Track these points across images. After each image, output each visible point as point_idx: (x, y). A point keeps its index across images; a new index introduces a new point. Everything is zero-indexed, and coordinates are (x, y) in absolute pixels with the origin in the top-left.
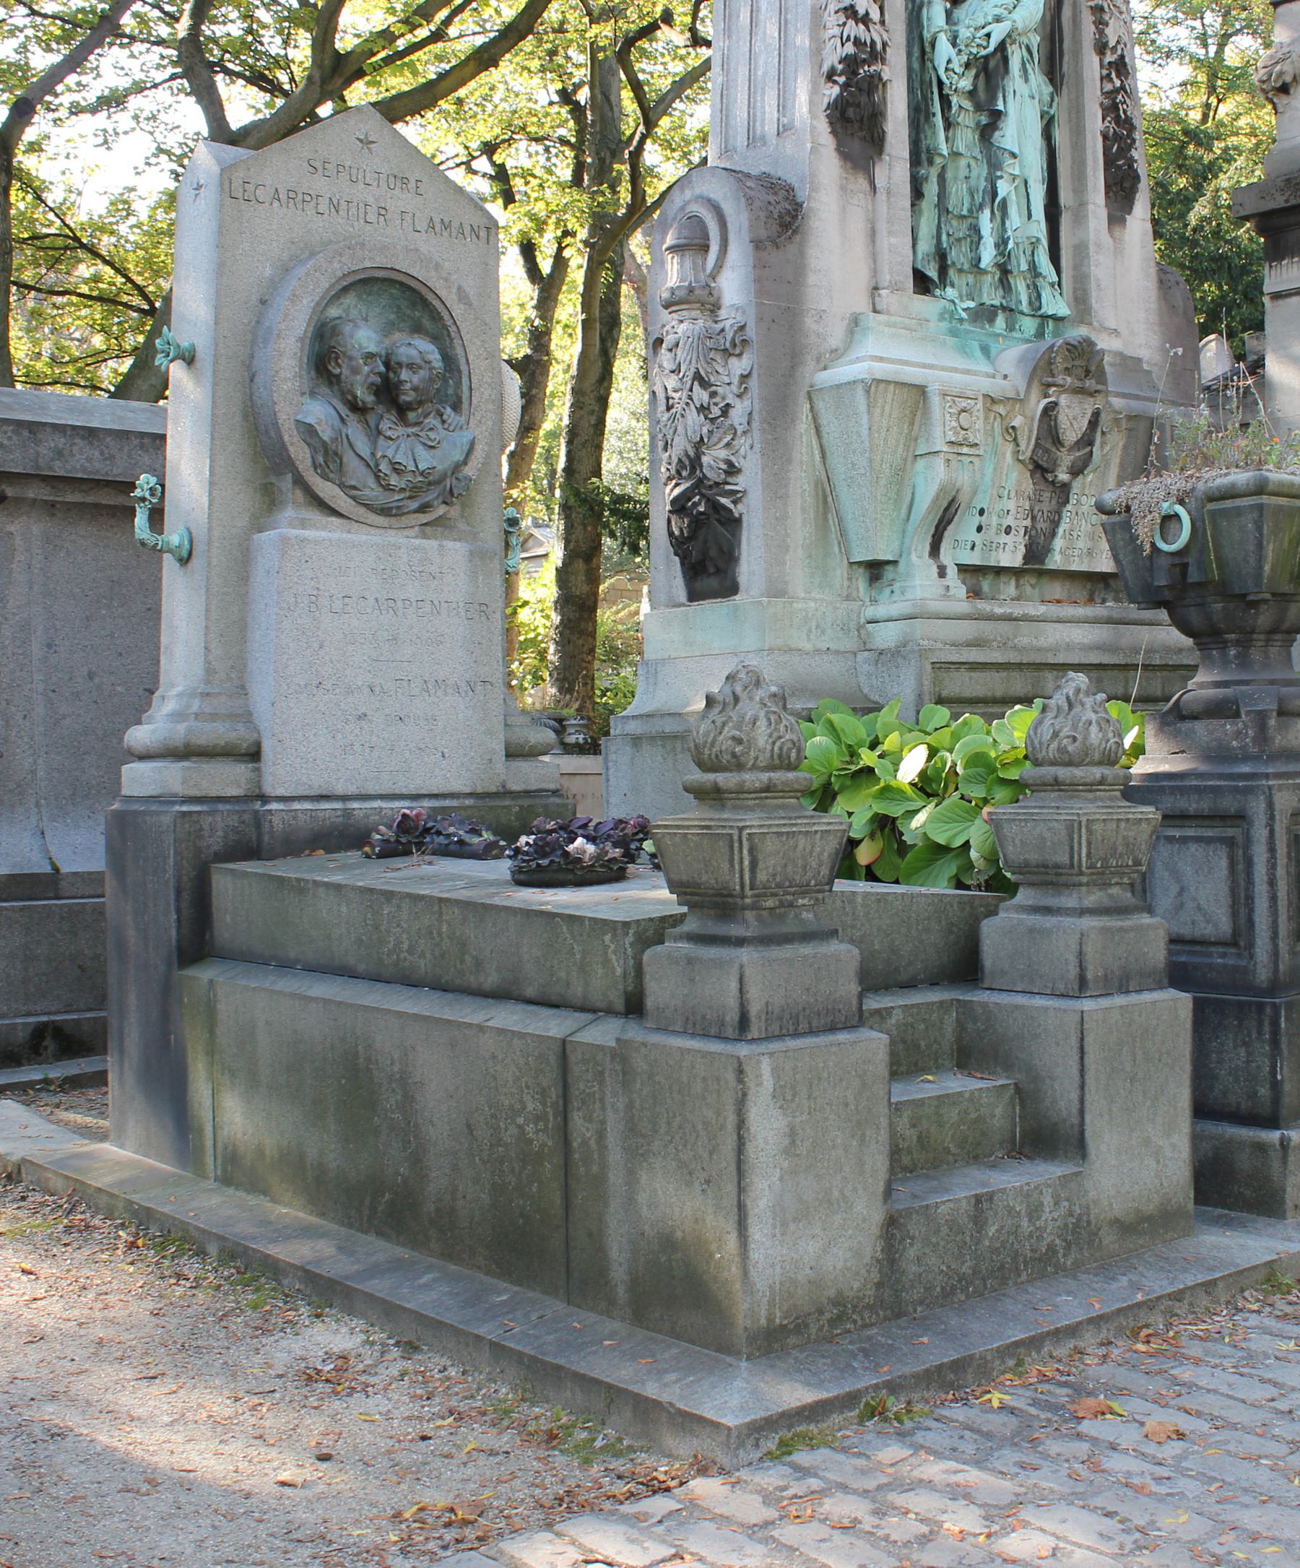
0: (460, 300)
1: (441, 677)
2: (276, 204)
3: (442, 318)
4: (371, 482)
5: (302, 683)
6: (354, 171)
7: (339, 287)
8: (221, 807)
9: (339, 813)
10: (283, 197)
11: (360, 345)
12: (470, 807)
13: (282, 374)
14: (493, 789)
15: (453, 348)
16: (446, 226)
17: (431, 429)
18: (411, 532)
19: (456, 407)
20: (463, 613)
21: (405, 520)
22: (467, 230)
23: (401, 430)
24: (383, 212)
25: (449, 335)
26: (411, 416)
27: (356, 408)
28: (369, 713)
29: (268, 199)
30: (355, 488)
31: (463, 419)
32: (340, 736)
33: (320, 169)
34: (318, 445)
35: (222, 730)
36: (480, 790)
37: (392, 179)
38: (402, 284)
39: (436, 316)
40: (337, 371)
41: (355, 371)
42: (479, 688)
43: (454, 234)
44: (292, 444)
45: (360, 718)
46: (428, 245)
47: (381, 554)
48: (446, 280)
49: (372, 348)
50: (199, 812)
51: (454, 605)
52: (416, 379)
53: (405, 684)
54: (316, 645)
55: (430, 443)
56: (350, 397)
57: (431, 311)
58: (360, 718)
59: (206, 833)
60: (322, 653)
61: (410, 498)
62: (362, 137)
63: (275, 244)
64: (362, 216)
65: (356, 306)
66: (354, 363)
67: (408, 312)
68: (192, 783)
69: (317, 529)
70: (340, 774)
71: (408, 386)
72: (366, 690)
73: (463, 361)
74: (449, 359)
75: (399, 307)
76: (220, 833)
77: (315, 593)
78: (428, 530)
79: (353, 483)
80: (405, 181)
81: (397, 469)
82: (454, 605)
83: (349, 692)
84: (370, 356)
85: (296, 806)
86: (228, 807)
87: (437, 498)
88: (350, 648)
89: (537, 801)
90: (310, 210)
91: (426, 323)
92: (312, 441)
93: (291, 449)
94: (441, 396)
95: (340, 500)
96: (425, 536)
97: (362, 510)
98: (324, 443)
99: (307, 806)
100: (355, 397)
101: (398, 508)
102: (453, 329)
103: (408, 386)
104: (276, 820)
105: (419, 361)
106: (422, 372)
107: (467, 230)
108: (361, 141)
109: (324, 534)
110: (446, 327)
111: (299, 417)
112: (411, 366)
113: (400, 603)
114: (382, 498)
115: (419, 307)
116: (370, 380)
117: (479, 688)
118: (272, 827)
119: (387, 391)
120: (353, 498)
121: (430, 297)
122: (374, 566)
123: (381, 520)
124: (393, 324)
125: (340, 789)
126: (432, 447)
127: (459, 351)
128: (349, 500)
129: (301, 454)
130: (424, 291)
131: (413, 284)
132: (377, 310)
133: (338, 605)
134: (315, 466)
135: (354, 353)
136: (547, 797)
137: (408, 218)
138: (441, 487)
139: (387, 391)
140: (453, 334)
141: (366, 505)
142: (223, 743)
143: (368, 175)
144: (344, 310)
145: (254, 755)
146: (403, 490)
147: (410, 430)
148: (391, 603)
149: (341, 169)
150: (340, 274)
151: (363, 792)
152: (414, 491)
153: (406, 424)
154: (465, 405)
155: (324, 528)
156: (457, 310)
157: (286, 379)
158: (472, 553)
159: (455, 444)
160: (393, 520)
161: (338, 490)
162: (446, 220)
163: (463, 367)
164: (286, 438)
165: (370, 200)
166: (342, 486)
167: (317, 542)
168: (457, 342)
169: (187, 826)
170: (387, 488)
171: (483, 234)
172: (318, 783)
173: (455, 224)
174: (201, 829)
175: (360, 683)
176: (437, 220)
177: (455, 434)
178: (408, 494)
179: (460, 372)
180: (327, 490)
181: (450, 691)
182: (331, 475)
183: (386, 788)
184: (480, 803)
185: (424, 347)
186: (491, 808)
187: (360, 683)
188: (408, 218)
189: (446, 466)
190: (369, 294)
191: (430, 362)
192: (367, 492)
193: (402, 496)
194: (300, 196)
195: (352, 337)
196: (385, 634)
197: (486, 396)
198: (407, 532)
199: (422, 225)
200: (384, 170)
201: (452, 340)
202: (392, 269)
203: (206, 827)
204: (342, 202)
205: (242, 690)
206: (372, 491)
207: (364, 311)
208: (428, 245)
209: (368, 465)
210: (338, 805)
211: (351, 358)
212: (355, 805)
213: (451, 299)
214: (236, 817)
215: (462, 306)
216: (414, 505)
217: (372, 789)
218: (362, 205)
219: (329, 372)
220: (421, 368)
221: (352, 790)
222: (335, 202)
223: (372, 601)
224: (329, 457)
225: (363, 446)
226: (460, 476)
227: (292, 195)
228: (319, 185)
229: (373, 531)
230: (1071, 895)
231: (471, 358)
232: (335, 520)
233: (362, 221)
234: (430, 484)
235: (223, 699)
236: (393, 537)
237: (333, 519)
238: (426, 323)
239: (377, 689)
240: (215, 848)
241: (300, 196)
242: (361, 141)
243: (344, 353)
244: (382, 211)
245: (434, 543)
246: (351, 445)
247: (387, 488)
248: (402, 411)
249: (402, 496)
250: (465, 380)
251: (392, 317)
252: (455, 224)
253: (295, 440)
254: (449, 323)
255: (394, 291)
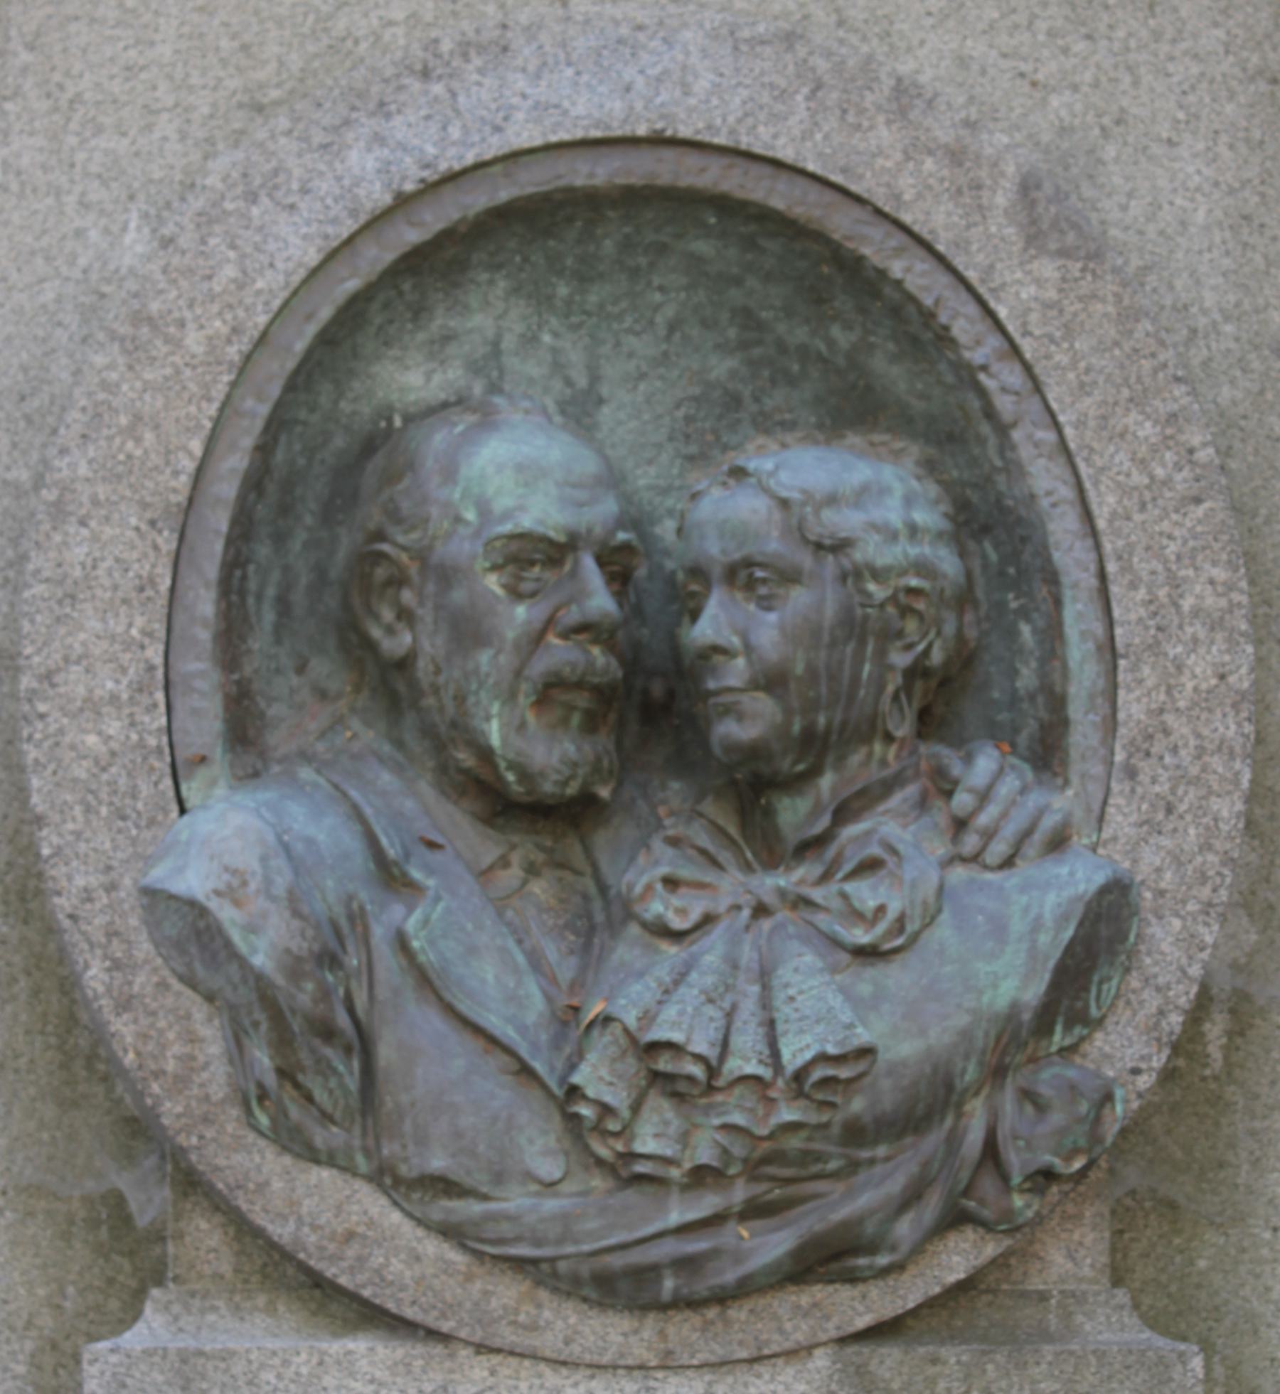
0: (1034, 238)
3: (944, 338)
4: (541, 1150)
7: (377, 256)
13: (75, 683)
15: (1014, 469)
17: (870, 866)
21: (746, 1324)
23: (733, 886)
25: (990, 413)
26: (793, 814)
30: (446, 1186)
31: (1061, 803)
34: (245, 995)
38: (725, 205)
39: (922, 335)
40: (397, 644)
41: (468, 631)
44: (125, 1004)
48: (956, 156)
49: (543, 513)
52: (769, 631)
55: (861, 936)
57: (895, 312)
61: (755, 1211)
63: (167, 126)
65: (530, 340)
66: (458, 596)
67: (800, 335)
73: (1062, 528)
74: (990, 521)
75: (746, 317)
79: (438, 1163)
81: (661, 1071)
84: (533, 556)
87: (911, 1198)
91: (893, 373)
92: (215, 982)
93: (123, 1028)
94: (943, 701)
95: (398, 1252)
97: (507, 1292)
98: (260, 983)
100: (486, 754)
101: (687, 1264)
102: (1002, 381)
103: (736, 672)
105: (774, 545)
110: (968, 376)
111: (158, 875)
112: (744, 575)
115: (843, 303)
116: (540, 666)
119: (647, 702)
120: (450, 1232)
121: (874, 246)
123: (609, 1331)
124: (734, 401)
127: (1044, 478)
128: (432, 1247)
130: (842, 223)
131: (779, 196)
132: (645, 346)
134: (252, 1097)
135: (461, 548)
138: (933, 1140)
139: (647, 702)
140: (1005, 405)
144: (474, 368)
146: (701, 1176)
147: (770, 883)
150: (377, 195)
152: (772, 1175)
153: (769, 849)
154: (1083, 732)
156: (1024, 288)
157: (92, 707)
159: (999, 929)
160: (683, 1327)
161: (371, 1204)
163: (1071, 557)
164: (95, 976)
166: (387, 1179)
168: (1029, 440)
170: (629, 1174)
177: (1010, 880)
178: (740, 1193)
179: (1052, 578)
180: (317, 1204)
182: (321, 1137)
185: (878, 499)
189: (940, 1035)
190: (583, 279)
191: (841, 546)
192: (515, 1200)
193: (707, 1203)
195: (450, 474)
197: (1201, 667)
201: (1003, 430)
202: (658, 141)
206: (541, 1186)
207: (575, 357)
209: (525, 1071)
215: (1048, 268)
216: (771, 1245)
219: (370, 645)
220: (790, 577)
225: (503, 984)
230: (741, 1307)
231: (1104, 505)
234: (855, 1133)
238: (893, 373)
243: (422, 556)
246: (426, 981)
247: (629, 1174)
249: (707, 1203)
250: (1078, 616)
251: (721, 367)
255: (703, 247)
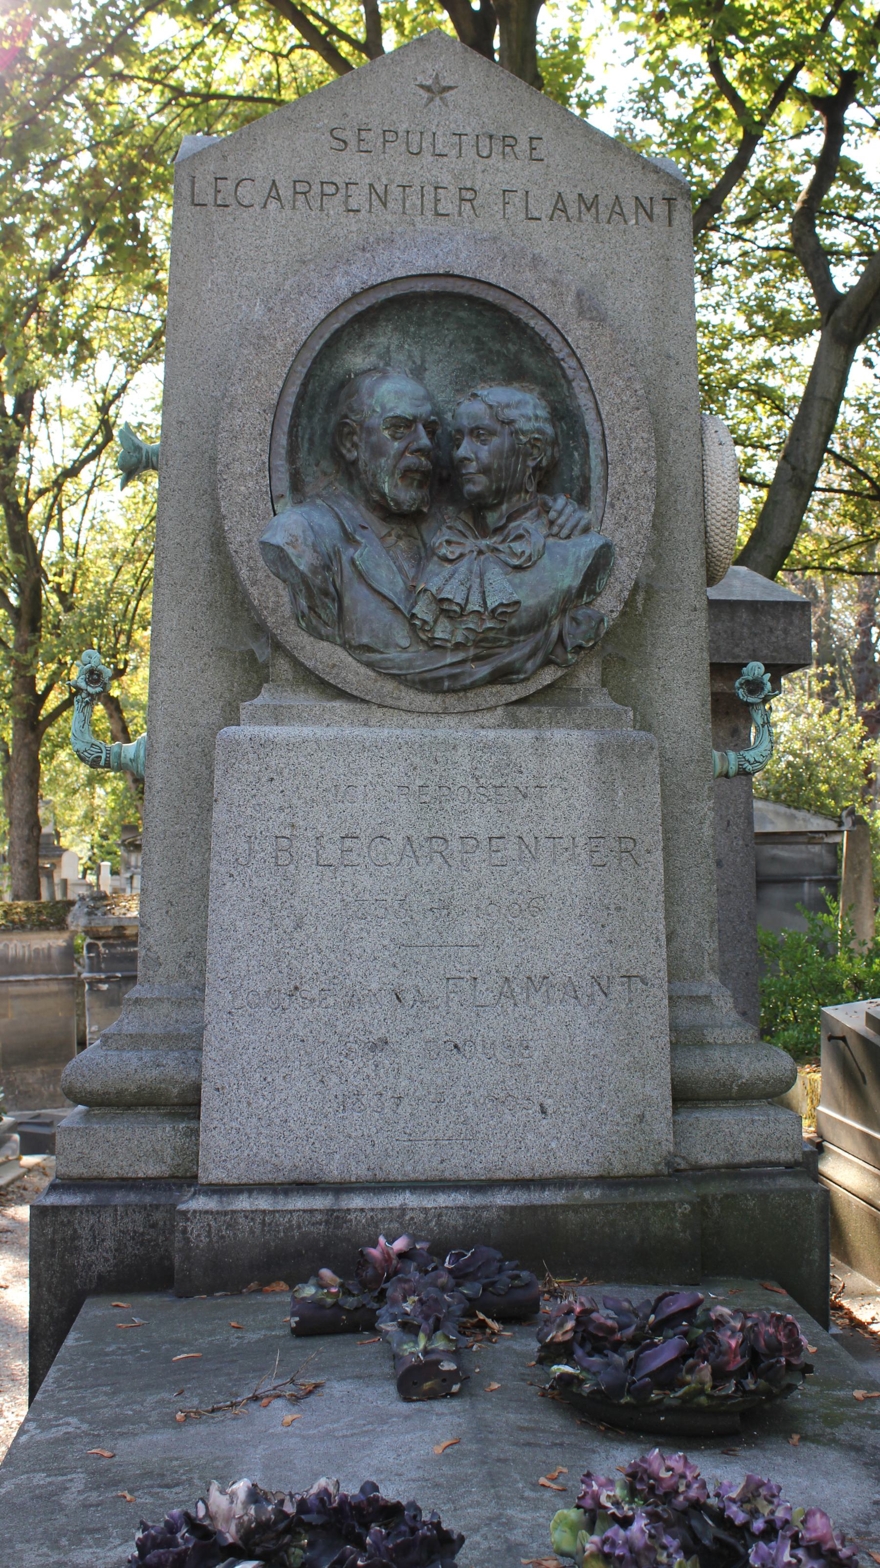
0: (581, 313)
1: (540, 969)
2: (273, 205)
3: (549, 349)
4: (402, 636)
5: (262, 989)
6: (415, 138)
8: (119, 1198)
9: (319, 1217)
10: (285, 192)
11: (383, 408)
12: (588, 1206)
13: (237, 468)
14: (647, 1168)
15: (573, 396)
16: (590, 205)
17: (519, 537)
18: (488, 718)
19: (583, 499)
20: (584, 856)
22: (629, 207)
23: (470, 544)
24: (469, 195)
25: (565, 376)
26: (492, 518)
27: (389, 513)
28: (392, 1039)
29: (259, 200)
30: (368, 648)
31: (587, 516)
32: (335, 1079)
33: (353, 143)
34: (297, 580)
35: (135, 1063)
36: (618, 1169)
37: (484, 142)
38: (472, 300)
39: (541, 348)
41: (377, 451)
42: (617, 989)
43: (604, 217)
44: (254, 583)
45: (374, 1047)
46: (549, 240)
47: (417, 760)
48: (554, 283)
49: (404, 409)
50: (73, 1208)
51: (566, 842)
53: (466, 985)
54: (289, 924)
56: (376, 497)
57: (531, 339)
58: (374, 1047)
59: (84, 1244)
60: (299, 936)
61: (477, 658)
62: (429, 82)
63: (270, 268)
64: (429, 205)
65: (400, 347)
66: (374, 438)
67: (497, 346)
68: (75, 1155)
69: (304, 722)
70: (333, 1146)
71: (473, 467)
72: (387, 999)
73: (589, 417)
74: (564, 415)
75: (478, 340)
76: (109, 1243)
77: (287, 832)
78: (523, 712)
79: (365, 640)
80: (508, 142)
81: (444, 608)
82: (566, 842)
83: (352, 1001)
85: (243, 1203)
86: (133, 1198)
87: (532, 655)
88: (355, 926)
89: (750, 1185)
90: (335, 206)
91: (529, 361)
92: (287, 575)
93: (254, 591)
94: (547, 479)
95: (352, 672)
96: (516, 723)
97: (389, 686)
98: (302, 575)
99: (263, 1203)
100: (383, 495)
101: (453, 677)
102: (569, 364)
103: (473, 467)
104: (195, 1229)
106: (495, 441)
107: (629, 207)
108: (428, 89)
109: (307, 731)
110: (557, 362)
111: (266, 537)
112: (476, 432)
113: (455, 844)
114: (424, 662)
116: (403, 464)
117: (617, 989)
118: (187, 1241)
119: (440, 478)
120: (369, 665)
121: (524, 315)
122: (405, 781)
123: (425, 700)
125: (334, 1171)
126: (518, 568)
127: (584, 400)
128: (363, 670)
129: (274, 599)
130: (513, 306)
131: (491, 296)
133: (331, 853)
134: (299, 616)
135: (375, 421)
136: (772, 1176)
137: (517, 199)
138: (540, 635)
139: (440, 478)
140: (570, 373)
141: (394, 676)
142: (133, 1088)
143: (440, 141)
144: (380, 357)
145: (187, 1106)
146: (458, 646)
147: (483, 543)
148: (437, 845)
149: (390, 137)
151: (380, 1176)
152: (484, 646)
153: (484, 531)
155: (318, 720)
156: (578, 332)
158: (601, 749)
159: (565, 560)
160: (451, 700)
161: (341, 655)
162: (589, 195)
164: (244, 573)
165: (445, 179)
166: (346, 645)
167: (290, 746)
168: (579, 385)
169: (49, 1230)
170: (432, 645)
171: (660, 209)
172: (290, 1158)
173: (606, 200)
174: (75, 1236)
175: (374, 986)
176: (570, 197)
177: (569, 543)
178: (472, 652)
179: (586, 435)
180: (322, 654)
181: (557, 995)
183: (426, 1165)
184: (615, 1196)
185: (525, 406)
186: (631, 1207)
187: (374, 986)
188: (517, 199)
189: (543, 597)
190: (420, 325)
191: (511, 422)
192: (392, 653)
193: (460, 656)
194: (316, 188)
195: (371, 395)
196: (426, 900)
197: (638, 468)
198: (478, 719)
199: (543, 207)
200: (471, 128)
201: (569, 382)
202: (447, 275)
203: (84, 1233)
204: (392, 188)
205: (196, 994)
207: (417, 353)
208: (549, 240)
209: (396, 608)
210: (320, 1202)
211: (370, 431)
212: (357, 1202)
213: (564, 314)
214: (139, 1217)
215: (586, 324)
216: (483, 671)
217: (397, 1168)
218: (429, 189)
219: (342, 456)
221: (358, 1171)
222: (380, 189)
223: (400, 841)
224: (322, 597)
225: (388, 577)
226: (580, 614)
227: (301, 188)
228: (353, 165)
229: (412, 720)
231: (605, 410)
232: (340, 706)
233: (429, 214)
234: (513, 632)
235: (165, 1008)
236: (449, 729)
237: (337, 704)
238: (529, 361)
239: (409, 997)
240: (100, 1268)
241: (316, 188)
242: (428, 89)
243: (361, 424)
244: (467, 195)
245: (527, 735)
246: (361, 576)
247: (432, 645)
248: (478, 512)
249: (460, 656)
250: (595, 450)
251: (469, 358)
252: (606, 200)
253: (260, 575)
254: (562, 353)
255: (462, 314)
